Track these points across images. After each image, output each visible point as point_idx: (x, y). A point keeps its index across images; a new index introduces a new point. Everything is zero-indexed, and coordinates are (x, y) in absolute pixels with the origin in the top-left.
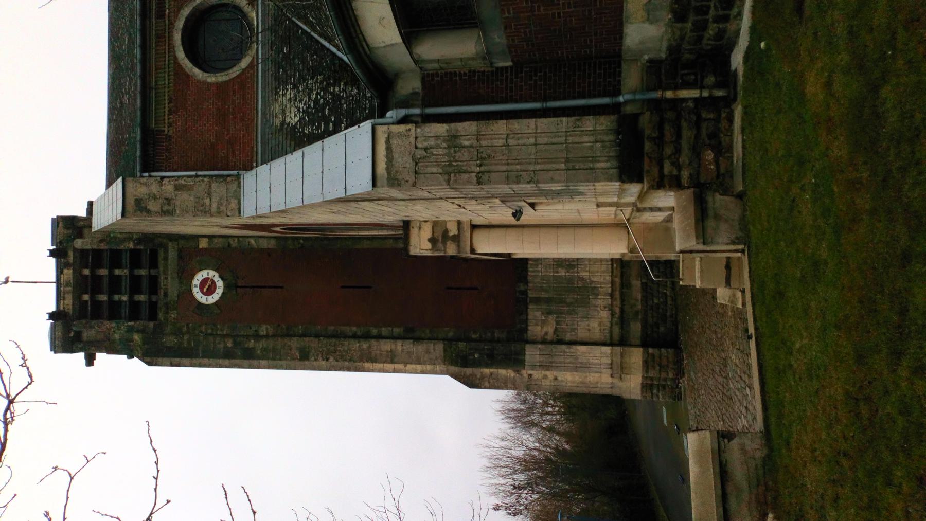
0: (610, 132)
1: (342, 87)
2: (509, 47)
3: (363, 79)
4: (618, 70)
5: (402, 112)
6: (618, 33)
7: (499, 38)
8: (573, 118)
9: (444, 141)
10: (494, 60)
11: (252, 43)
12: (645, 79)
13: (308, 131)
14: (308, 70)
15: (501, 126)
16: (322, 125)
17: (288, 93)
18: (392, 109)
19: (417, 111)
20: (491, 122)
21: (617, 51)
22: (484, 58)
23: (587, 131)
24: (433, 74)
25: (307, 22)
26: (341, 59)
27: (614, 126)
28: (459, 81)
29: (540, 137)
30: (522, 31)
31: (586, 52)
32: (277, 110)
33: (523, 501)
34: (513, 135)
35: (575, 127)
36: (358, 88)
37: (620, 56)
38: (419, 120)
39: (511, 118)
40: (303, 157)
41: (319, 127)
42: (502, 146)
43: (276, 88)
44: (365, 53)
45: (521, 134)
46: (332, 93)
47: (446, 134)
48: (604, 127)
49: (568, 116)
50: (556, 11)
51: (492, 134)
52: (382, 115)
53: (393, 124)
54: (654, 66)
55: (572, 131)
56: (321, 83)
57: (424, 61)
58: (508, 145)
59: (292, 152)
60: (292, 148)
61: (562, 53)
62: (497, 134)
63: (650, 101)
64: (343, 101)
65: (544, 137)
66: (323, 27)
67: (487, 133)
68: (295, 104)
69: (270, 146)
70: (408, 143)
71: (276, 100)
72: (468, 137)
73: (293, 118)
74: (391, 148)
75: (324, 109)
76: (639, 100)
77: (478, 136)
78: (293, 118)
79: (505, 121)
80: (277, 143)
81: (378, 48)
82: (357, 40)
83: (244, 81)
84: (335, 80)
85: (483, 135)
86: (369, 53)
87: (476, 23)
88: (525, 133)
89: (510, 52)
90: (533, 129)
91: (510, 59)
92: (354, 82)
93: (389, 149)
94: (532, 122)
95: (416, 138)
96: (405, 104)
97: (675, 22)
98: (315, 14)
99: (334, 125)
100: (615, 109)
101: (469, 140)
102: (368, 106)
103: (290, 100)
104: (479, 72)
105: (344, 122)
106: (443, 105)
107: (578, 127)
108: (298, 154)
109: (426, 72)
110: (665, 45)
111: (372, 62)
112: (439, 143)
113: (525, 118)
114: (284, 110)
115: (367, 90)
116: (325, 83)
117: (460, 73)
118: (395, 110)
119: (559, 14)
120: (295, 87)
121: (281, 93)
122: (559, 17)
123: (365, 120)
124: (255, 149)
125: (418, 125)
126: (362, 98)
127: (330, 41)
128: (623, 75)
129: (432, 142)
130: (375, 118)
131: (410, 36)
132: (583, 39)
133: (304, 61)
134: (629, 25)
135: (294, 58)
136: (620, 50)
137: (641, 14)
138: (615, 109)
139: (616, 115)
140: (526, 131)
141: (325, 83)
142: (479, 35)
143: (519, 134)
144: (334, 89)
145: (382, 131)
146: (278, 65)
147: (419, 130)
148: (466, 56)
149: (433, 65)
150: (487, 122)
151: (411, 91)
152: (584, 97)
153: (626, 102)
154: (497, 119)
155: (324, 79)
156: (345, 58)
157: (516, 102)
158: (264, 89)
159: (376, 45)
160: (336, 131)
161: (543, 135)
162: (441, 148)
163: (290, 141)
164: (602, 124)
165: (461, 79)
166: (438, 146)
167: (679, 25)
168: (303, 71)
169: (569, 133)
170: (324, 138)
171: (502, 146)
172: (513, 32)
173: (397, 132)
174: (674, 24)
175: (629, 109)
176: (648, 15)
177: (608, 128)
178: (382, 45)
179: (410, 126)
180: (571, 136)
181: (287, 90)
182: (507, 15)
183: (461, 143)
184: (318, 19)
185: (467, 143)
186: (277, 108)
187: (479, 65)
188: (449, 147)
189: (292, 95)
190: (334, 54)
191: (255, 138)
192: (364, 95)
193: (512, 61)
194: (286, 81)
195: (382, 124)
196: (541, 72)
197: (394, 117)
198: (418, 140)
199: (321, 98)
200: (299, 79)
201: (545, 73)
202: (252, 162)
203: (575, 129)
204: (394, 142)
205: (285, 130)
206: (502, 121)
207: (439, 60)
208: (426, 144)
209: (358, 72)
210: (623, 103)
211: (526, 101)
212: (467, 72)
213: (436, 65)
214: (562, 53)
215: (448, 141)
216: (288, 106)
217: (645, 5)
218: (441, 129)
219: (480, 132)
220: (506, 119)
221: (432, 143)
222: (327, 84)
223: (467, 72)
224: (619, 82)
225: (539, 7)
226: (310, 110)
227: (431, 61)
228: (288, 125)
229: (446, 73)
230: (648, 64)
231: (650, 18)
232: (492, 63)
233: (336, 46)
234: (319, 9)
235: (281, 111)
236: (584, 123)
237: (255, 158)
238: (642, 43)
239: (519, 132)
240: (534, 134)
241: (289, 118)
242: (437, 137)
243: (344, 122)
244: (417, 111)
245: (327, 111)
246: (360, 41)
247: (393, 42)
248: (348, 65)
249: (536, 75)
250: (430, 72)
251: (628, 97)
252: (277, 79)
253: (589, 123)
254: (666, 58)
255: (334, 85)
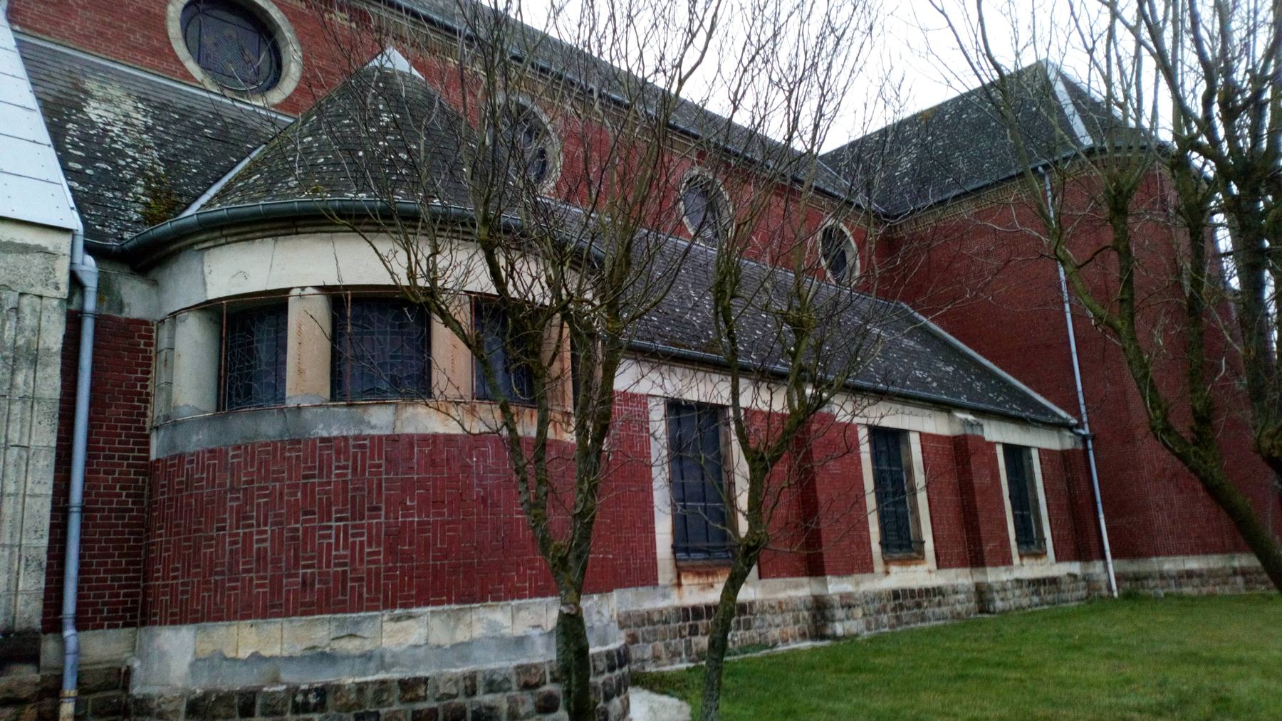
0: (10, 619)
1: (144, 198)
2: (181, 457)
3: (155, 231)
4: (121, 622)
5: (91, 282)
6: (179, 618)
7: (197, 441)
8: (44, 557)
9: (29, 343)
10: (162, 433)
11: (222, 87)
12: (100, 667)
13: (70, 129)
14: (175, 155)
15: (45, 437)
16: (79, 153)
17: (139, 116)
18: (97, 266)
19: (90, 305)
20: (56, 421)
21: (153, 619)
22: (167, 417)
23: (17, 580)
24: (151, 337)
25: (249, 172)
26: (188, 206)
27: (20, 624)
28: (133, 376)
29: (16, 503)
30: (205, 475)
31: (158, 571)
32: (112, 92)
33: (878, 689)
34: (25, 457)
35: (27, 560)
36: (138, 222)
37: (143, 624)
38: (74, 307)
39: (58, 455)
40: (24, 107)
41: (76, 146)
42: (6, 437)
43: (148, 100)
44: (197, 243)
45: (27, 471)
46: (133, 181)
47: (41, 346)
48: (20, 607)
49: (50, 549)
50: (228, 524)
51: (31, 422)
52: (89, 249)
53: (72, 263)
54: (122, 677)
55: (20, 556)
56: (152, 169)
57: (174, 326)
58: (6, 448)
59: (35, 92)
60: (41, 96)
61: (160, 535)
62: (30, 430)
63: (59, 680)
64: (118, 194)
65: (15, 508)
66: (241, 191)
67: (35, 414)
68: (120, 120)
69: (49, 62)
70: (33, 282)
71: (129, 95)
72: (32, 383)
73: (96, 112)
74: (27, 253)
75: (107, 162)
76: (63, 661)
77: (31, 400)
78: (94, 111)
79: (54, 444)
80: (53, 74)
81: (202, 262)
82: (217, 234)
83: (162, 55)
84: (155, 191)
85: (32, 407)
86: (196, 248)
87: (224, 409)
88: (26, 478)
89: (173, 458)
90: (32, 490)
91: (161, 457)
92: (150, 219)
93: (25, 249)
94: (47, 489)
95: (41, 297)
96: (104, 288)
97: (188, 701)
98: (261, 185)
99: (77, 171)
100: (53, 623)
101: (26, 383)
102: (107, 230)
103: (127, 115)
104: (146, 408)
105: (81, 188)
106: (96, 347)
107: (27, 565)
108: (32, 102)
109: (155, 328)
110: (153, 690)
111: (180, 251)
112: (27, 333)
113: (56, 478)
114: (110, 101)
115: (135, 234)
116: (151, 174)
117: (148, 379)
118: (96, 270)
119: (223, 528)
120: (148, 129)
121: (140, 105)
122: (219, 529)
123: (84, 221)
124: (45, 37)
125: (65, 304)
126: (122, 224)
127: (221, 196)
128: (111, 631)
129: (29, 321)
130: (85, 236)
131: (210, 309)
132: (179, 565)
133: (188, 153)
134: (192, 632)
135: (194, 140)
136: (154, 623)
137: (207, 648)
138: (53, 623)
139: (40, 627)
140: (30, 479)
141: (151, 174)
142: (205, 412)
143: (27, 465)
144: (141, 185)
145: (64, 242)
146: (185, 114)
147: (55, 303)
148: (174, 390)
149: (166, 340)
150: (57, 415)
151: (126, 300)
152: (80, 572)
153: (62, 642)
154: (59, 431)
155: (158, 175)
156: (188, 213)
157: (87, 464)
158: (149, 82)
159: (206, 258)
160: (67, 171)
161: (20, 507)
162: (16, 335)
163: (55, 97)
164: (27, 604)
165: (137, 379)
166: (19, 330)
167: (183, 708)
168: (173, 148)
169: (17, 549)
170: (57, 149)
171: (6, 437)
172: (203, 463)
173: (56, 266)
174: (185, 700)
175: (49, 647)
176: (205, 660)
177: (18, 616)
178: (206, 270)
179: (64, 290)
180: (11, 554)
181: (145, 116)
182: (231, 453)
183: (21, 370)
184: (254, 187)
185: (20, 379)
186: (115, 91)
187: (157, 409)
188: (15, 348)
189: (136, 122)
190: (196, 198)
191: (64, 43)
192: (127, 229)
193: (158, 460)
194: (158, 119)
195: (72, 245)
196: (133, 503)
197: (84, 268)
198: (37, 300)
199: (127, 163)
200: (161, 139)
201: (132, 510)
202: (20, 25)
203: (23, 562)
204: (37, 260)
205: (75, 93)
206: (55, 439)
207: (173, 349)
208: (27, 310)
209: (168, 226)
210: (61, 636)
211: (86, 480)
212: (148, 390)
213: (164, 343)
214: (160, 535)
215: (28, 349)
216: (118, 111)
217: (221, 653)
218: (54, 338)
219: (39, 403)
220: (58, 447)
221: (27, 322)
222: (149, 178)
223: (148, 390)
224: (101, 627)
225: (238, 499)
226: (108, 140)
227: (172, 337)
228: (84, 101)
229: (150, 359)
230: (123, 670)
231: (197, 663)
232: (157, 428)
233: (210, 203)
234: (268, 191)
235: (110, 97)
236: (33, 574)
237: (27, 31)
238: (162, 655)
239: (30, 467)
240: (22, 492)
241: (97, 105)
242: (38, 331)
243: (81, 188)
244: (90, 305)
245: (103, 166)
246: (215, 239)
247: (209, 286)
248: (176, 215)
249: (127, 496)
250: (154, 335)
251: (71, 644)
252: (163, 107)
253: (33, 582)
254: (129, 696)
255: (147, 187)
